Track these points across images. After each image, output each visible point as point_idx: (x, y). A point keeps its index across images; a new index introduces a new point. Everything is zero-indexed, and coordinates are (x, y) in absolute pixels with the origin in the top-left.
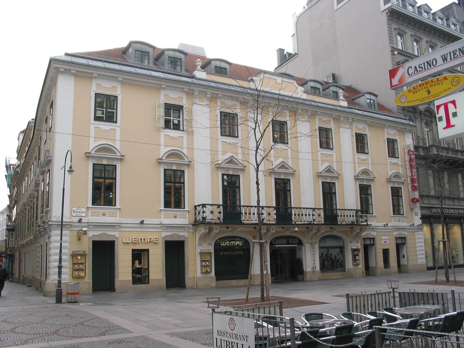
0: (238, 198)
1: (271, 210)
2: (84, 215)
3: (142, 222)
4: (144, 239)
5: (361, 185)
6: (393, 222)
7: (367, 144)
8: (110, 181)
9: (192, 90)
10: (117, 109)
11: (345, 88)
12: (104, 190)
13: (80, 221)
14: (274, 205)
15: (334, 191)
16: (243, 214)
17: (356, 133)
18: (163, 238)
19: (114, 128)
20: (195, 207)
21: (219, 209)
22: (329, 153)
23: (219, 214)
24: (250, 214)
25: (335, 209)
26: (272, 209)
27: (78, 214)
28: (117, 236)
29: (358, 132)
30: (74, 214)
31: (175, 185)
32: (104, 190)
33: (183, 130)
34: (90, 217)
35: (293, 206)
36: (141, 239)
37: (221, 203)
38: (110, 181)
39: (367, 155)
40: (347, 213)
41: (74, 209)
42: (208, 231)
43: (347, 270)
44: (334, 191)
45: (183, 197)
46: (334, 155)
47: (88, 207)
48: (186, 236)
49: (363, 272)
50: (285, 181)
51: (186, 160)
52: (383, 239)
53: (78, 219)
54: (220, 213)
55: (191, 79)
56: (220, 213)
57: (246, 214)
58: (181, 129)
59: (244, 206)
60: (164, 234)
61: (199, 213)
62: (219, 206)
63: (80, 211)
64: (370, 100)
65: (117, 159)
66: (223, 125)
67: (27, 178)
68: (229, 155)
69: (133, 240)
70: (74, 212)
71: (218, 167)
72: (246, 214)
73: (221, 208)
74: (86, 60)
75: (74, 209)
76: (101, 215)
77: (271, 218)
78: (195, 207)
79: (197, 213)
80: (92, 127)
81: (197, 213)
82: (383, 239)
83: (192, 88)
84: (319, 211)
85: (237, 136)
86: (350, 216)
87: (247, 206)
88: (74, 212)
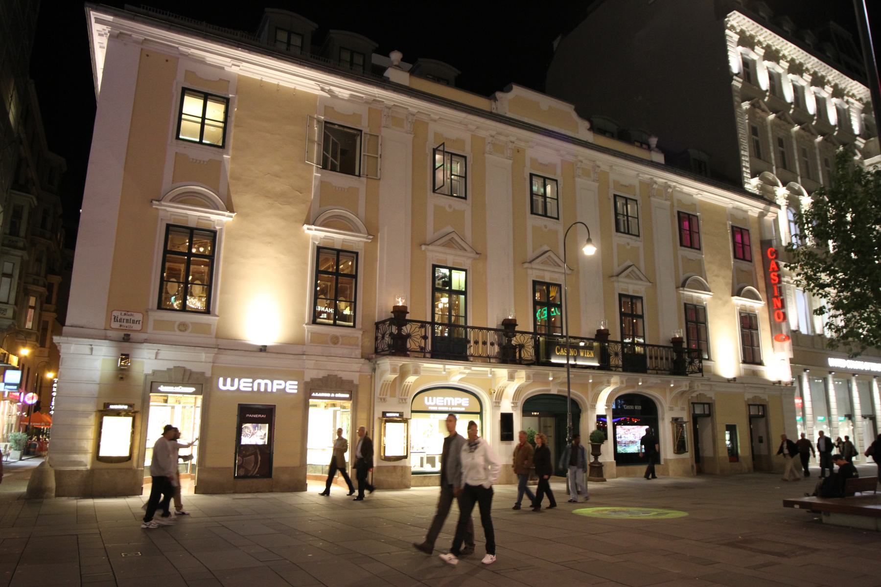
1: (526, 338)
2: (137, 327)
16: (472, 343)
20: (377, 324)
21: (423, 330)
23: (423, 341)
24: (484, 343)
25: (462, 326)
27: (125, 324)
30: (115, 325)
33: (359, 176)
35: (470, 323)
39: (638, 238)
41: (115, 313)
43: (662, 462)
44: (702, 320)
49: (692, 466)
52: (422, 466)
54: (425, 338)
58: (357, 173)
59: (473, 328)
61: (383, 338)
63: (128, 318)
75: (115, 313)
82: (422, 466)
84: (522, 338)
87: (481, 329)
88: (116, 319)
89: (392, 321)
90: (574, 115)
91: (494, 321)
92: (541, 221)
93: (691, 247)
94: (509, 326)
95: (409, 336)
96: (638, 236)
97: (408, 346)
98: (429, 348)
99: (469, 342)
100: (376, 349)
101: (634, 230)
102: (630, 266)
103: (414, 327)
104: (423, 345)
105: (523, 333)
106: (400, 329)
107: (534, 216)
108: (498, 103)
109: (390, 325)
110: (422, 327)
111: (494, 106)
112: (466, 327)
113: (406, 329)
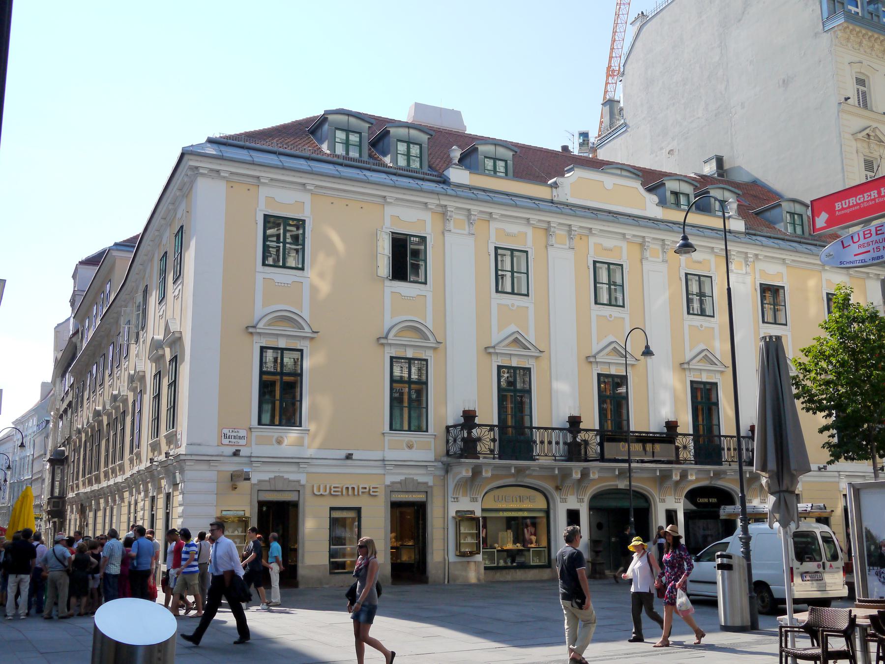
0: (625, 417)
1: (591, 435)
3: (349, 457)
4: (353, 488)
5: (695, 386)
6: (253, 443)
7: (527, 274)
8: (292, 379)
9: (442, 206)
10: (303, 245)
11: (640, 174)
12: (280, 395)
13: (236, 454)
14: (597, 427)
15: (714, 400)
17: (761, 284)
18: (388, 486)
19: (300, 280)
21: (492, 433)
22: (705, 324)
24: (550, 443)
25: (528, 428)
26: (591, 434)
27: (233, 440)
28: (303, 482)
29: (270, 212)
30: (226, 441)
31: (281, 378)
32: (280, 395)
34: (254, 446)
36: (347, 488)
37: (496, 423)
38: (292, 379)
40: (550, 436)
41: (226, 431)
42: (470, 474)
44: (714, 400)
45: (298, 403)
46: (430, 296)
47: (250, 429)
48: (430, 484)
50: (708, 387)
51: (307, 329)
53: (233, 449)
54: (494, 440)
55: (442, 186)
56: (494, 440)
57: (542, 442)
59: (726, 437)
60: (389, 480)
61: (455, 441)
62: (492, 428)
63: (235, 434)
64: (495, 160)
65: (304, 338)
66: (612, 287)
67: (95, 367)
68: (513, 328)
69: (333, 489)
70: (225, 436)
71: (489, 351)
72: (542, 442)
73: (496, 429)
74: (245, 152)
76: (274, 442)
77: (484, 449)
78: (448, 428)
79: (451, 439)
80: (259, 278)
81: (451, 439)
83: (443, 203)
84: (587, 436)
85: (524, 291)
86: (550, 443)
87: (546, 429)
88: (225, 436)
89: (463, 426)
90: (641, 189)
91: (560, 418)
92: (698, 320)
93: (703, 313)
94: (574, 422)
95: (479, 439)
96: (786, 325)
97: (479, 449)
98: (496, 452)
99: (724, 449)
100: (448, 451)
101: (708, 312)
102: (613, 342)
103: (484, 430)
104: (492, 447)
105: (587, 430)
106: (469, 433)
107: (499, 294)
108: (559, 189)
109: (462, 429)
110: (491, 430)
111: (555, 193)
112: (531, 428)
113: (475, 432)
